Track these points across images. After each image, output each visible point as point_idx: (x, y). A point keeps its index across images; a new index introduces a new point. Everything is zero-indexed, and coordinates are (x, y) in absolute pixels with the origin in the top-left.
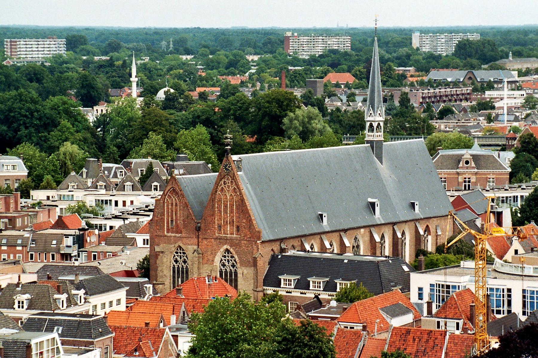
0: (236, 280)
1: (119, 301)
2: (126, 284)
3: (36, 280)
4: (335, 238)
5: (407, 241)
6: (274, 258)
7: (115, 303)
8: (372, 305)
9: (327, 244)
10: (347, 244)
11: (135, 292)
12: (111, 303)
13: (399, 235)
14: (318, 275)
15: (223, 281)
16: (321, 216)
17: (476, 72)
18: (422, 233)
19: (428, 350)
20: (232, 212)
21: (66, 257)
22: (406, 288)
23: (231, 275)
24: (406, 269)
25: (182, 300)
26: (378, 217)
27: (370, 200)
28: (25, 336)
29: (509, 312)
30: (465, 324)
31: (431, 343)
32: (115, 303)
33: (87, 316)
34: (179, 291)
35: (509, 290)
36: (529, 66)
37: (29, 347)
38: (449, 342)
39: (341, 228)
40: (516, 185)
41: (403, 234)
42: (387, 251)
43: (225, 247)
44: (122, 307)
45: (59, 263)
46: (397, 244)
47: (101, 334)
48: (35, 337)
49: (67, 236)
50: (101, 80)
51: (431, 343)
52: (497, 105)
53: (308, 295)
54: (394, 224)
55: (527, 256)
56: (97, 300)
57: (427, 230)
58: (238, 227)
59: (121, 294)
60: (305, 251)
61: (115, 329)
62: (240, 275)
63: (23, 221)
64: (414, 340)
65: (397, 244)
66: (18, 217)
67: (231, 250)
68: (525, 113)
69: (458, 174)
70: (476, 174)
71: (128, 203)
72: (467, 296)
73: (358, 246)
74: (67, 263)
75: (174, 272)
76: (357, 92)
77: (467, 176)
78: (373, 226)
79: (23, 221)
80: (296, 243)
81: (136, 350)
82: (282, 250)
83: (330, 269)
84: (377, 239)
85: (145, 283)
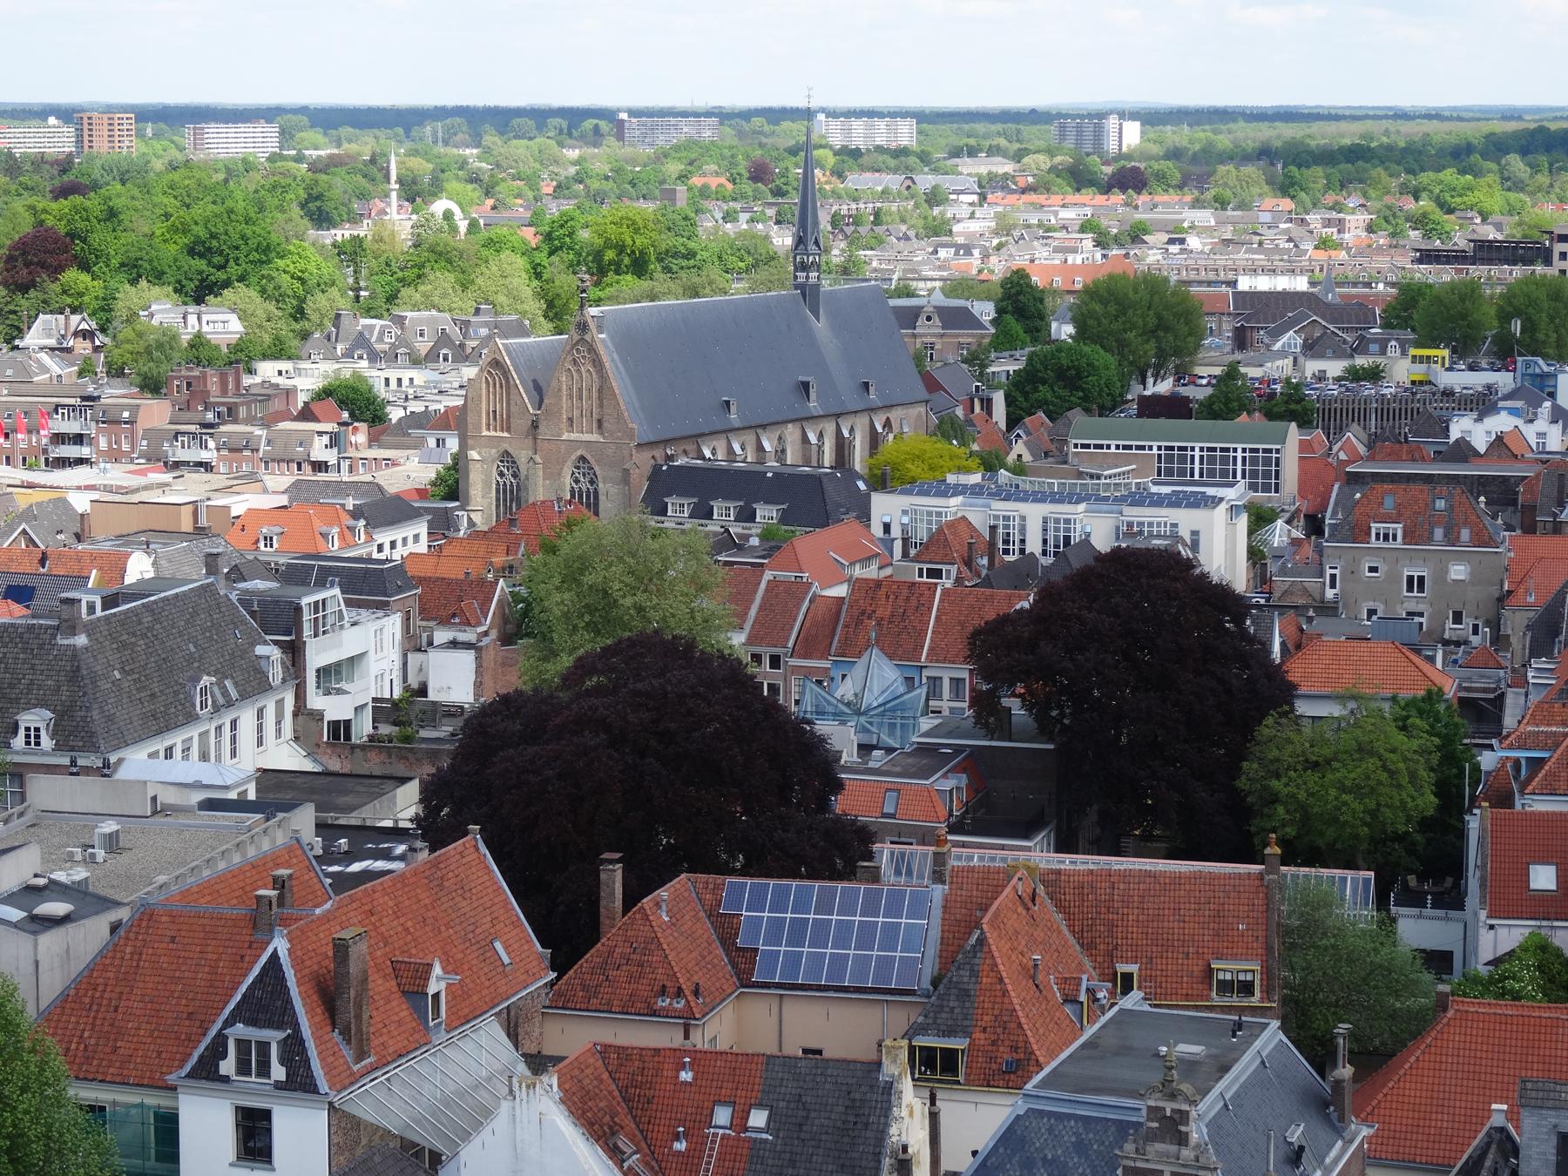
0: (596, 505)
1: (416, 538)
2: (428, 510)
3: (286, 503)
4: (750, 438)
5: (858, 443)
6: (656, 469)
7: (410, 540)
8: (810, 544)
9: (737, 448)
10: (767, 446)
11: (442, 525)
12: (405, 540)
13: (846, 435)
14: (726, 498)
15: (583, 508)
16: (728, 403)
17: (917, 178)
18: (880, 430)
19: (1458, 213)
20: (590, 398)
21: (320, 466)
22: (865, 516)
23: (588, 497)
24: (861, 485)
25: (518, 538)
26: (813, 405)
27: (801, 378)
28: (291, 592)
29: (1022, 551)
30: (959, 571)
31: (914, 602)
32: (410, 540)
33: (370, 560)
34: (512, 522)
35: (1023, 518)
36: (994, 169)
37: (298, 609)
38: (941, 601)
39: (759, 422)
40: (1006, 354)
41: (852, 430)
42: (828, 458)
43: (579, 453)
44: (422, 547)
45: (308, 474)
46: (842, 447)
47: (400, 590)
48: (306, 594)
49: (320, 433)
50: (337, 185)
51: (914, 602)
52: (956, 228)
53: (710, 528)
54: (838, 415)
55: (1037, 464)
56: (384, 537)
57: (888, 424)
58: (600, 422)
59: (422, 528)
60: (704, 458)
61: (421, 581)
62: (602, 498)
63: (249, 409)
64: (888, 597)
65: (842, 447)
66: (243, 404)
67: (588, 457)
68: (995, 242)
69: (914, 336)
70: (942, 336)
71: (406, 382)
72: (962, 527)
73: (783, 451)
74: (322, 477)
75: (498, 491)
76: (738, 206)
77: (929, 340)
78: (807, 419)
79: (249, 409)
80: (691, 447)
81: (454, 615)
82: (670, 458)
83: (746, 487)
84: (813, 438)
85: (456, 509)
